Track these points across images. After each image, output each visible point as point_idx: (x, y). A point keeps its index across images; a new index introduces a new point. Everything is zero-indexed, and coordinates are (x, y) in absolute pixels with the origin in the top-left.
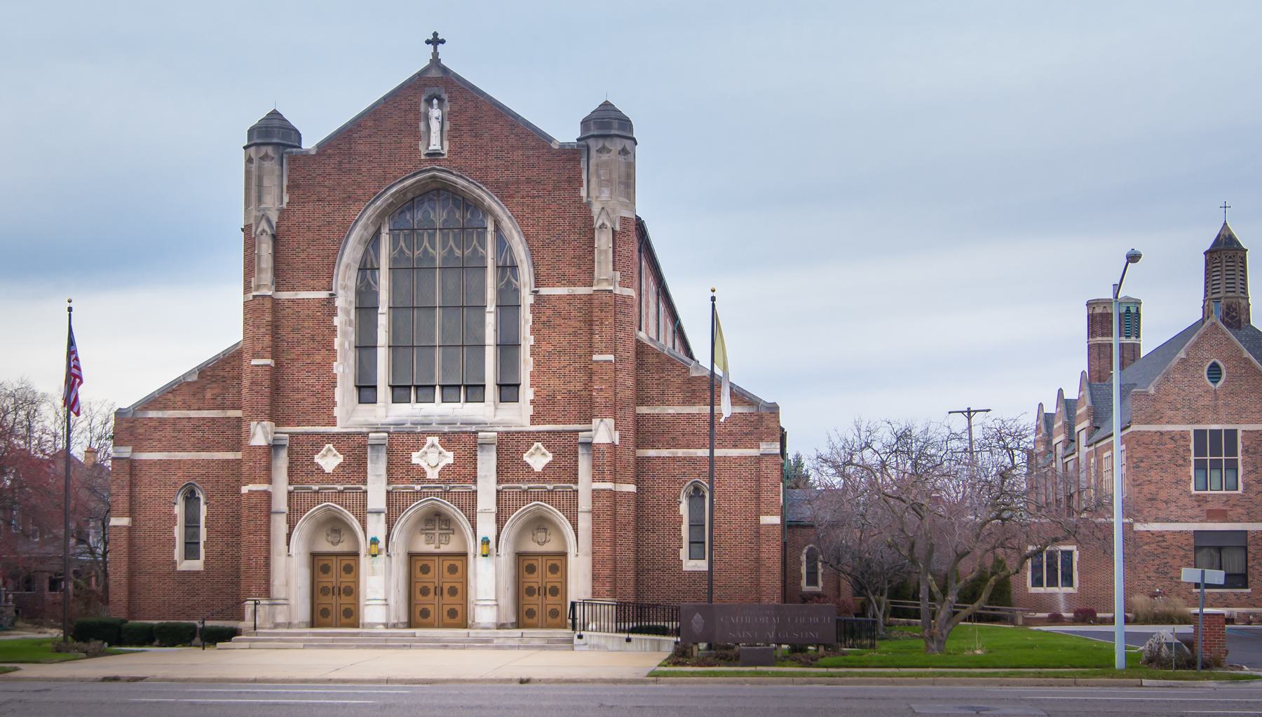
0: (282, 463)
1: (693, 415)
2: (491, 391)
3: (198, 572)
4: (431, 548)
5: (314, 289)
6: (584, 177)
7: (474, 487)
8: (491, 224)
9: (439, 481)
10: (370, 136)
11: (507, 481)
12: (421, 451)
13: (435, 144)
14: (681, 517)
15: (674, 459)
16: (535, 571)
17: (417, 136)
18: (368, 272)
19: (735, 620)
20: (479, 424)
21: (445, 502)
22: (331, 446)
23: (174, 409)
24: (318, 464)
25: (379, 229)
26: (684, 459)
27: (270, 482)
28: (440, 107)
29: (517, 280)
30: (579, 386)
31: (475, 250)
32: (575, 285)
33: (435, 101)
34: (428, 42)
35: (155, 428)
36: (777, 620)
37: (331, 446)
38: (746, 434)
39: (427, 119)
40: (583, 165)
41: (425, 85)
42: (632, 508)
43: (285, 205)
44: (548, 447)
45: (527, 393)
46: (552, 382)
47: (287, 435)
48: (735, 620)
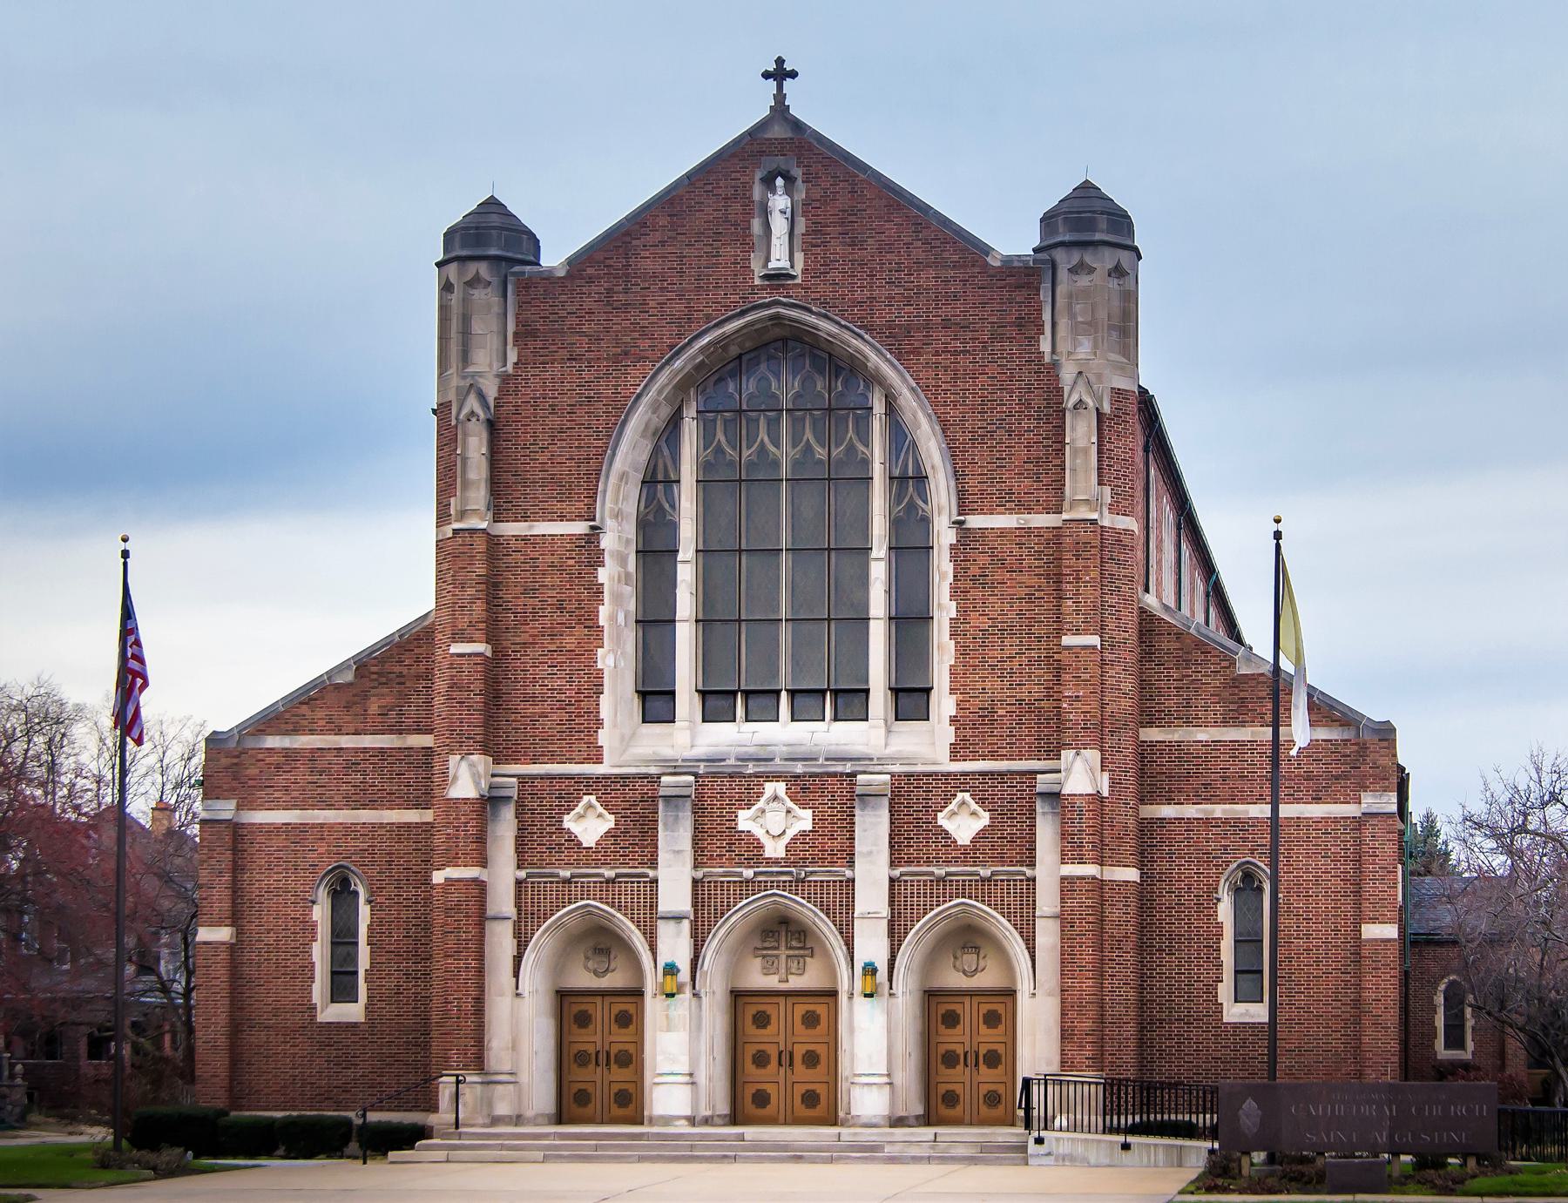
0: (505, 828)
1: (1242, 743)
2: (879, 700)
3: (355, 1025)
4: (772, 982)
5: (562, 518)
6: (1047, 316)
7: (848, 873)
8: (880, 401)
9: (786, 862)
10: (663, 243)
11: (909, 862)
12: (754, 808)
13: (779, 258)
14: (1220, 926)
15: (1207, 822)
16: (958, 1023)
17: (746, 242)
18: (660, 487)
19: (1317, 1110)
20: (858, 759)
21: (786, 894)
22: (593, 798)
23: (312, 732)
24: (569, 832)
25: (680, 409)
26: (1226, 821)
27: (483, 862)
28: (789, 191)
29: (926, 502)
30: (1037, 692)
31: (851, 448)
32: (1029, 510)
33: (780, 182)
34: (766, 75)
35: (278, 767)
36: (1391, 1111)
37: (593, 798)
38: (1337, 778)
39: (765, 213)
40: (1045, 295)
41: (762, 153)
42: (1132, 910)
43: (510, 368)
44: (981, 801)
45: (944, 704)
46: (988, 685)
47: (889, 777)
48: (1317, 1110)
